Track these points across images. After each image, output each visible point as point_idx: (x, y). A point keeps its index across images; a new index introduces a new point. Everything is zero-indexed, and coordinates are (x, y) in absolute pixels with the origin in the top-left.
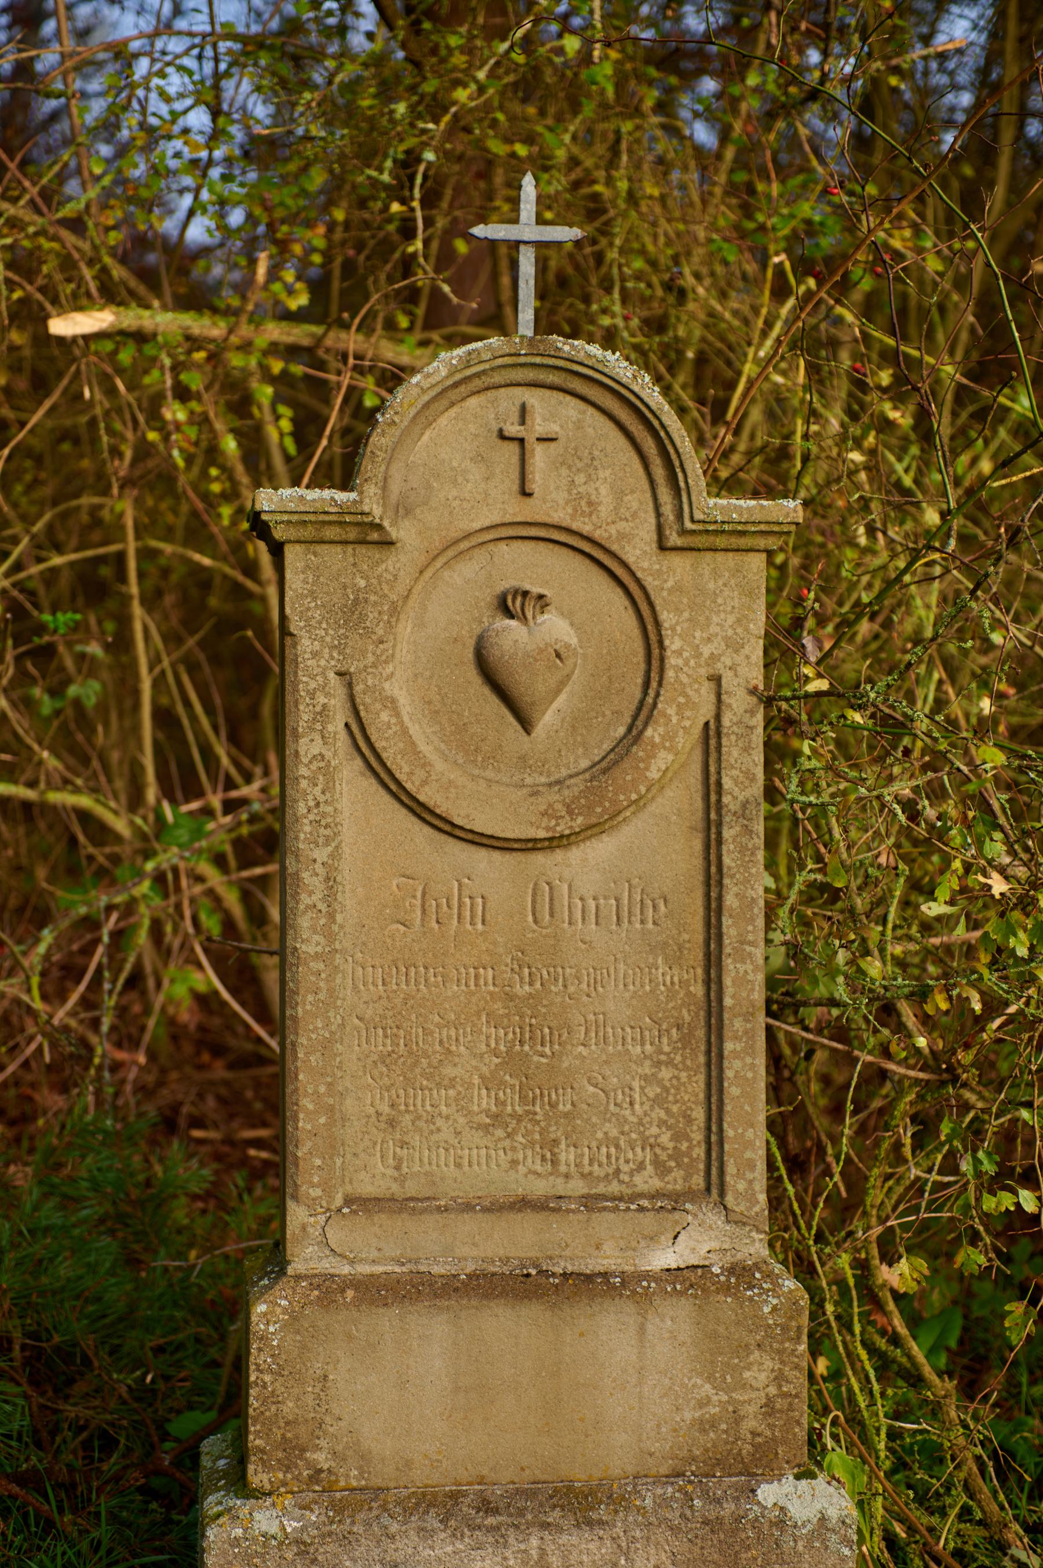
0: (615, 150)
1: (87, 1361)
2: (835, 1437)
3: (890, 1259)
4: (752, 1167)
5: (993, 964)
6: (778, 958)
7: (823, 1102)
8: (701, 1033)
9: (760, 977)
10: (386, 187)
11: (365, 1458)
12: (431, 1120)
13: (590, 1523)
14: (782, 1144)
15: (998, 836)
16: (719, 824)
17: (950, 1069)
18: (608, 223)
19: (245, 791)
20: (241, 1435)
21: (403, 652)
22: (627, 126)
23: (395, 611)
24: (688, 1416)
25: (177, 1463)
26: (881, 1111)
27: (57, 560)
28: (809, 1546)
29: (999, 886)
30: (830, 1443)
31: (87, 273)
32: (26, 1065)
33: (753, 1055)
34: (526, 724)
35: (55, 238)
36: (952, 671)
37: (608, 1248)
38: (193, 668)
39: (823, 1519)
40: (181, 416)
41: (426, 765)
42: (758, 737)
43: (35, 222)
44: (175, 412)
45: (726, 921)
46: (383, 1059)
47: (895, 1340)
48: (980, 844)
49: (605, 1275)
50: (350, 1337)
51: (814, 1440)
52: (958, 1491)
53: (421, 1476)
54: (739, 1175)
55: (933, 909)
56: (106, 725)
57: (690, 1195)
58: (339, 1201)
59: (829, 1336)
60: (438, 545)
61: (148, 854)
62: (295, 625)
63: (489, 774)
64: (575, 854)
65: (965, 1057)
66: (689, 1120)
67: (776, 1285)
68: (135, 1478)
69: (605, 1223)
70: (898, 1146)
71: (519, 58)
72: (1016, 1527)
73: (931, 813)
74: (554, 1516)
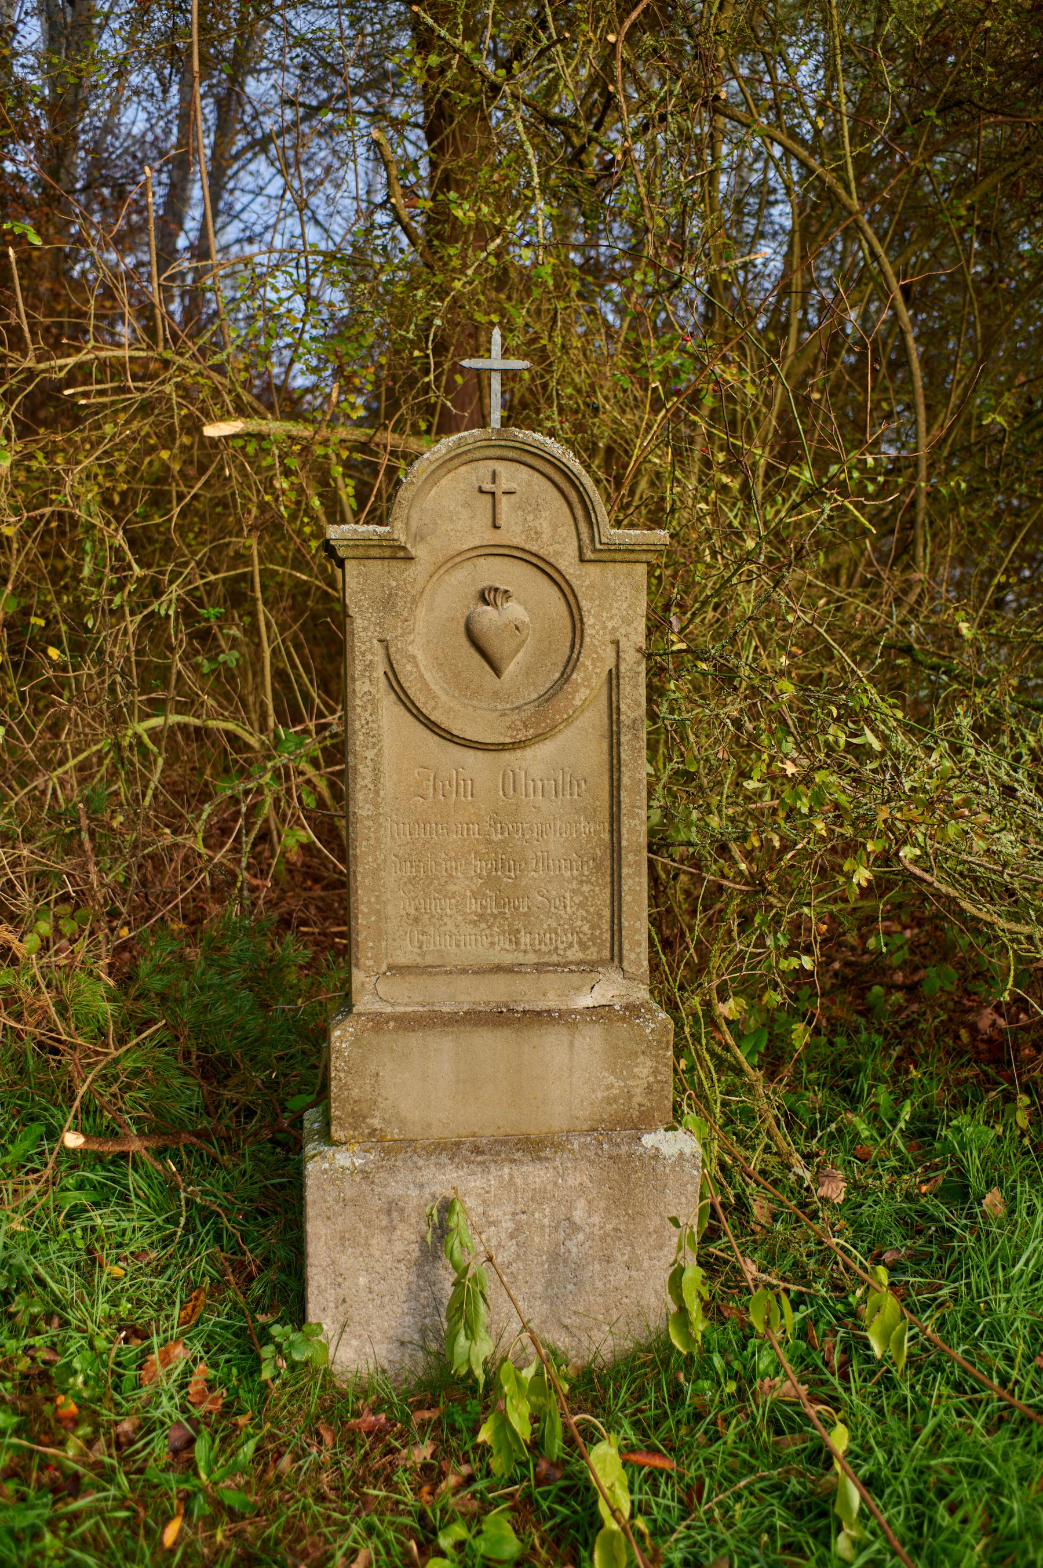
0: (554, 320)
1: (236, 1066)
2: (689, 1106)
3: (723, 999)
4: (639, 945)
5: (788, 817)
6: (657, 816)
7: (685, 906)
8: (608, 863)
9: (644, 829)
10: (411, 341)
11: (402, 1123)
12: (441, 918)
13: (540, 1159)
14: (659, 931)
15: (790, 739)
16: (619, 733)
17: (761, 884)
18: (550, 365)
19: (329, 719)
20: (328, 1109)
21: (420, 627)
22: (561, 305)
23: (415, 601)
24: (600, 1095)
25: (292, 1125)
26: (721, 911)
27: (212, 577)
28: (673, 1170)
29: (790, 769)
30: (686, 1109)
31: (227, 398)
32: (198, 887)
33: (640, 876)
34: (497, 671)
35: (208, 377)
36: (764, 641)
37: (551, 995)
38: (298, 647)
39: (681, 1154)
40: (285, 485)
41: (435, 697)
42: (642, 680)
43: (195, 367)
44: (282, 483)
45: (623, 794)
46: (410, 880)
47: (727, 1048)
48: (779, 743)
49: (549, 1011)
50: (392, 1050)
51: (676, 1108)
52: (763, 1136)
53: (437, 1133)
54: (632, 950)
55: (751, 785)
56: (245, 680)
57: (601, 962)
58: (384, 968)
59: (686, 1046)
60: (441, 559)
61: (269, 758)
62: (352, 610)
63: (475, 703)
64: (529, 752)
65: (770, 876)
66: (601, 917)
67: (654, 1016)
68: (266, 1134)
69: (549, 979)
70: (729, 931)
71: (492, 260)
72: (797, 1156)
73: (749, 726)
74: (518, 1155)
